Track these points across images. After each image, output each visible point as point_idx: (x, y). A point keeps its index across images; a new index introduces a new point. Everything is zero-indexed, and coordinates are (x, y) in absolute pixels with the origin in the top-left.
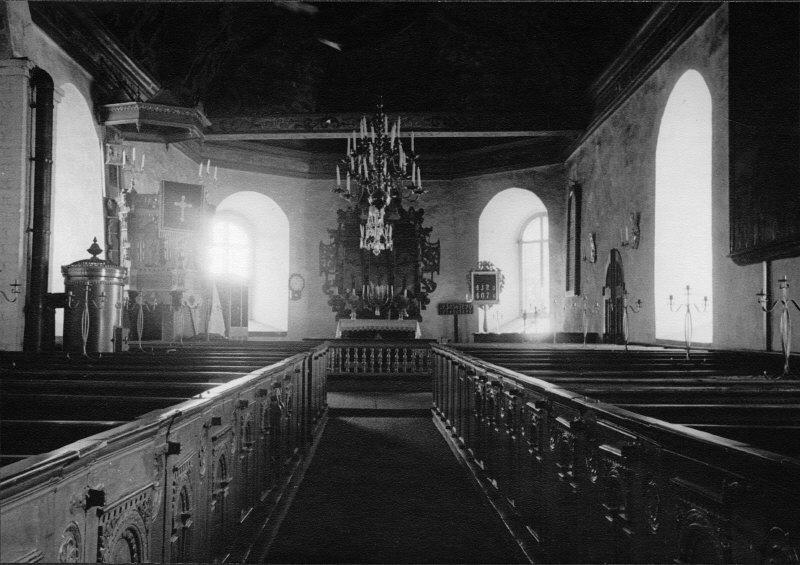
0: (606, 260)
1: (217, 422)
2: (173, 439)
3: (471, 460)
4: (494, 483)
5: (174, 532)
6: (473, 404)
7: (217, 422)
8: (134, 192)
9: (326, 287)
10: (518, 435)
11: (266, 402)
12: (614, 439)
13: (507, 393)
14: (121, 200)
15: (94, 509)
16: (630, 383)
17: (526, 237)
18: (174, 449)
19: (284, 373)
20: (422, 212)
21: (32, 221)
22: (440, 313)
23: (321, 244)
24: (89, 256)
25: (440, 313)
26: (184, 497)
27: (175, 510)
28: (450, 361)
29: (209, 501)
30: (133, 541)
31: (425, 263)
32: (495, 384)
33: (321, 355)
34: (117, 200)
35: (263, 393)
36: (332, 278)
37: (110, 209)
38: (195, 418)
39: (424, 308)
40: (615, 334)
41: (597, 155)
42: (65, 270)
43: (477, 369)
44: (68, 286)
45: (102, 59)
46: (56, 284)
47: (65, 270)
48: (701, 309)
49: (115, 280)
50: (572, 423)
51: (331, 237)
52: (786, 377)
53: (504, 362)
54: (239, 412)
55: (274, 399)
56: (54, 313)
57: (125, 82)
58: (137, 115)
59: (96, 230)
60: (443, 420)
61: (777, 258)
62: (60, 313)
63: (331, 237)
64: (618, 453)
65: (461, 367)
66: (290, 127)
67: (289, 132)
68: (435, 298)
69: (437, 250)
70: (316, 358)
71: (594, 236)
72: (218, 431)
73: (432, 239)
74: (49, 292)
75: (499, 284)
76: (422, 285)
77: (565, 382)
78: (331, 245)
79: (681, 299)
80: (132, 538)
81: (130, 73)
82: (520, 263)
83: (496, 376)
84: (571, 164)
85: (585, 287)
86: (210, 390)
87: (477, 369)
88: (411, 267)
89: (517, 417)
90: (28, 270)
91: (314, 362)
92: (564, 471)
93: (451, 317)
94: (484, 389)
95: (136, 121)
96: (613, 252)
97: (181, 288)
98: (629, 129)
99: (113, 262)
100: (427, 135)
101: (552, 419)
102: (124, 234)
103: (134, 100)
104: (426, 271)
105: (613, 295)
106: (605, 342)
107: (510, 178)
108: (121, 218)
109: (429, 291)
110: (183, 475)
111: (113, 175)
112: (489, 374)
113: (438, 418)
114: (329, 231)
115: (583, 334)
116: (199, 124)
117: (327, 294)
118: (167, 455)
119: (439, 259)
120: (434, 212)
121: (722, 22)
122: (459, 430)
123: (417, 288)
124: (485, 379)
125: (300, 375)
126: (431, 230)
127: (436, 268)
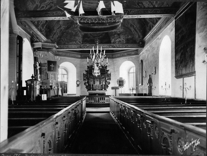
0: (147, 72)
1: (64, 117)
2: (56, 121)
3: (119, 123)
4: (124, 128)
5: (57, 141)
6: (119, 110)
7: (64, 117)
8: (41, 63)
9: (85, 84)
10: (129, 117)
11: (74, 111)
12: (149, 119)
13: (127, 109)
14: (38, 65)
15: (43, 137)
16: (153, 106)
17: (131, 72)
18: (57, 123)
19: (77, 105)
20: (107, 66)
21: (18, 71)
22: (112, 89)
23: (84, 74)
24: (31, 78)
25: (112, 89)
26: (59, 133)
27: (57, 136)
28: (114, 101)
29: (63, 134)
30: (50, 143)
31: (107, 78)
32: (124, 106)
33: (84, 100)
34: (37, 65)
35: (73, 109)
36: (86, 81)
37: (35, 67)
38: (60, 116)
39: (107, 88)
40: (150, 94)
41: (146, 54)
42: (26, 82)
43: (120, 103)
44: (27, 85)
45: (33, 32)
46: (24, 85)
47: (26, 82)
48: (168, 89)
49: (38, 84)
50: (141, 116)
51: (86, 72)
52: (186, 104)
53: (126, 101)
54: (68, 114)
55: (75, 110)
56: (24, 92)
57: (38, 37)
58: (41, 45)
59: (32, 72)
60: (112, 114)
61: (185, 77)
62: (25, 91)
63: (86, 72)
64: (150, 122)
65: (116, 102)
66: (76, 47)
67: (76, 48)
68: (110, 86)
69: (110, 75)
70: (84, 100)
71: (146, 72)
72: (65, 119)
73: (109, 72)
74: (43, 99)
75: (124, 82)
76: (107, 83)
77: (139, 106)
78: (86, 74)
79: (164, 87)
80: (50, 143)
81: (39, 35)
82: (129, 77)
83: (124, 105)
84: (140, 56)
85: (144, 83)
86: (62, 110)
87: (120, 103)
88: (104, 79)
89: (129, 114)
90: (17, 81)
91: (83, 101)
92: (139, 125)
93: (115, 90)
94: (122, 107)
95: (41, 47)
96: (150, 75)
97: (52, 85)
98: (153, 48)
99: (36, 80)
100: (108, 49)
101: (136, 115)
102: (39, 73)
103: (40, 42)
104: (107, 80)
105: (150, 85)
106: (148, 96)
107: (127, 58)
108: (38, 69)
109: (108, 84)
110: (58, 128)
111: (36, 59)
112: (123, 104)
113: (111, 113)
114: (86, 71)
115: (143, 94)
116: (55, 47)
117: (85, 85)
118: (55, 125)
119: (111, 77)
120: (110, 66)
121: (173, 25)
122: (116, 116)
123: (106, 83)
124: (122, 105)
125: (80, 105)
126: (109, 70)
127: (110, 79)
